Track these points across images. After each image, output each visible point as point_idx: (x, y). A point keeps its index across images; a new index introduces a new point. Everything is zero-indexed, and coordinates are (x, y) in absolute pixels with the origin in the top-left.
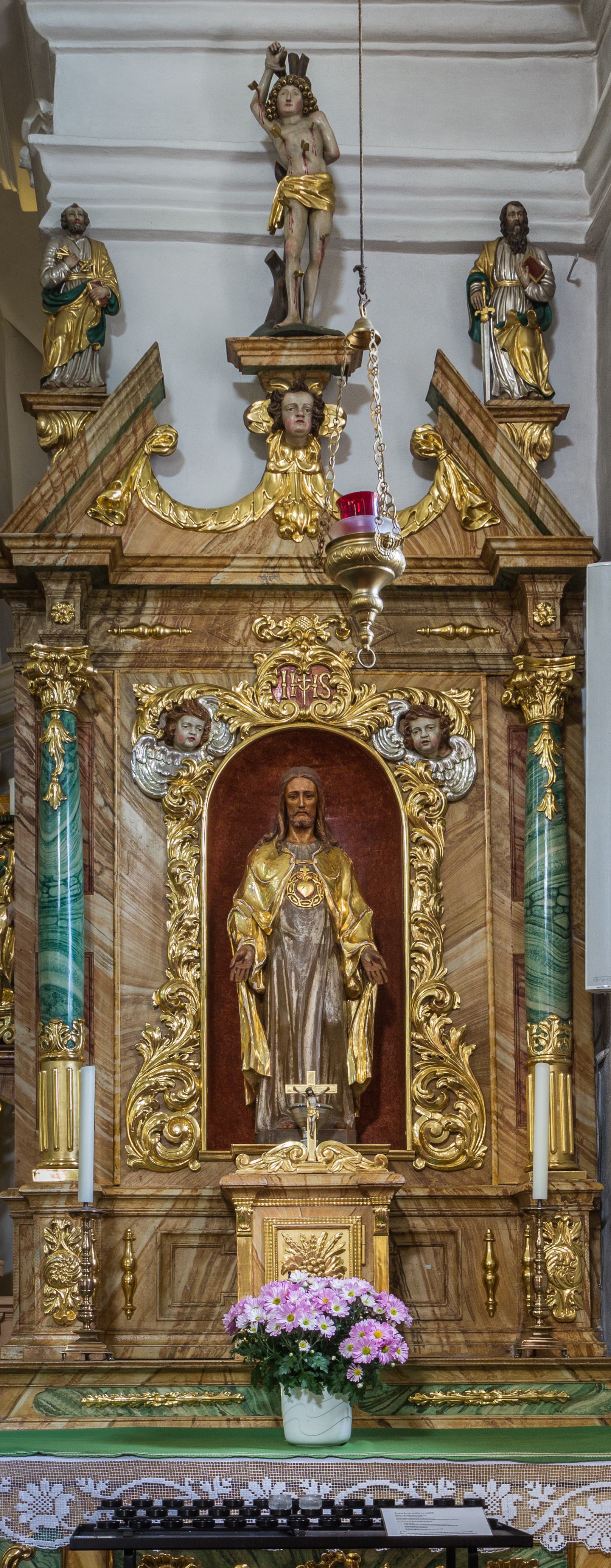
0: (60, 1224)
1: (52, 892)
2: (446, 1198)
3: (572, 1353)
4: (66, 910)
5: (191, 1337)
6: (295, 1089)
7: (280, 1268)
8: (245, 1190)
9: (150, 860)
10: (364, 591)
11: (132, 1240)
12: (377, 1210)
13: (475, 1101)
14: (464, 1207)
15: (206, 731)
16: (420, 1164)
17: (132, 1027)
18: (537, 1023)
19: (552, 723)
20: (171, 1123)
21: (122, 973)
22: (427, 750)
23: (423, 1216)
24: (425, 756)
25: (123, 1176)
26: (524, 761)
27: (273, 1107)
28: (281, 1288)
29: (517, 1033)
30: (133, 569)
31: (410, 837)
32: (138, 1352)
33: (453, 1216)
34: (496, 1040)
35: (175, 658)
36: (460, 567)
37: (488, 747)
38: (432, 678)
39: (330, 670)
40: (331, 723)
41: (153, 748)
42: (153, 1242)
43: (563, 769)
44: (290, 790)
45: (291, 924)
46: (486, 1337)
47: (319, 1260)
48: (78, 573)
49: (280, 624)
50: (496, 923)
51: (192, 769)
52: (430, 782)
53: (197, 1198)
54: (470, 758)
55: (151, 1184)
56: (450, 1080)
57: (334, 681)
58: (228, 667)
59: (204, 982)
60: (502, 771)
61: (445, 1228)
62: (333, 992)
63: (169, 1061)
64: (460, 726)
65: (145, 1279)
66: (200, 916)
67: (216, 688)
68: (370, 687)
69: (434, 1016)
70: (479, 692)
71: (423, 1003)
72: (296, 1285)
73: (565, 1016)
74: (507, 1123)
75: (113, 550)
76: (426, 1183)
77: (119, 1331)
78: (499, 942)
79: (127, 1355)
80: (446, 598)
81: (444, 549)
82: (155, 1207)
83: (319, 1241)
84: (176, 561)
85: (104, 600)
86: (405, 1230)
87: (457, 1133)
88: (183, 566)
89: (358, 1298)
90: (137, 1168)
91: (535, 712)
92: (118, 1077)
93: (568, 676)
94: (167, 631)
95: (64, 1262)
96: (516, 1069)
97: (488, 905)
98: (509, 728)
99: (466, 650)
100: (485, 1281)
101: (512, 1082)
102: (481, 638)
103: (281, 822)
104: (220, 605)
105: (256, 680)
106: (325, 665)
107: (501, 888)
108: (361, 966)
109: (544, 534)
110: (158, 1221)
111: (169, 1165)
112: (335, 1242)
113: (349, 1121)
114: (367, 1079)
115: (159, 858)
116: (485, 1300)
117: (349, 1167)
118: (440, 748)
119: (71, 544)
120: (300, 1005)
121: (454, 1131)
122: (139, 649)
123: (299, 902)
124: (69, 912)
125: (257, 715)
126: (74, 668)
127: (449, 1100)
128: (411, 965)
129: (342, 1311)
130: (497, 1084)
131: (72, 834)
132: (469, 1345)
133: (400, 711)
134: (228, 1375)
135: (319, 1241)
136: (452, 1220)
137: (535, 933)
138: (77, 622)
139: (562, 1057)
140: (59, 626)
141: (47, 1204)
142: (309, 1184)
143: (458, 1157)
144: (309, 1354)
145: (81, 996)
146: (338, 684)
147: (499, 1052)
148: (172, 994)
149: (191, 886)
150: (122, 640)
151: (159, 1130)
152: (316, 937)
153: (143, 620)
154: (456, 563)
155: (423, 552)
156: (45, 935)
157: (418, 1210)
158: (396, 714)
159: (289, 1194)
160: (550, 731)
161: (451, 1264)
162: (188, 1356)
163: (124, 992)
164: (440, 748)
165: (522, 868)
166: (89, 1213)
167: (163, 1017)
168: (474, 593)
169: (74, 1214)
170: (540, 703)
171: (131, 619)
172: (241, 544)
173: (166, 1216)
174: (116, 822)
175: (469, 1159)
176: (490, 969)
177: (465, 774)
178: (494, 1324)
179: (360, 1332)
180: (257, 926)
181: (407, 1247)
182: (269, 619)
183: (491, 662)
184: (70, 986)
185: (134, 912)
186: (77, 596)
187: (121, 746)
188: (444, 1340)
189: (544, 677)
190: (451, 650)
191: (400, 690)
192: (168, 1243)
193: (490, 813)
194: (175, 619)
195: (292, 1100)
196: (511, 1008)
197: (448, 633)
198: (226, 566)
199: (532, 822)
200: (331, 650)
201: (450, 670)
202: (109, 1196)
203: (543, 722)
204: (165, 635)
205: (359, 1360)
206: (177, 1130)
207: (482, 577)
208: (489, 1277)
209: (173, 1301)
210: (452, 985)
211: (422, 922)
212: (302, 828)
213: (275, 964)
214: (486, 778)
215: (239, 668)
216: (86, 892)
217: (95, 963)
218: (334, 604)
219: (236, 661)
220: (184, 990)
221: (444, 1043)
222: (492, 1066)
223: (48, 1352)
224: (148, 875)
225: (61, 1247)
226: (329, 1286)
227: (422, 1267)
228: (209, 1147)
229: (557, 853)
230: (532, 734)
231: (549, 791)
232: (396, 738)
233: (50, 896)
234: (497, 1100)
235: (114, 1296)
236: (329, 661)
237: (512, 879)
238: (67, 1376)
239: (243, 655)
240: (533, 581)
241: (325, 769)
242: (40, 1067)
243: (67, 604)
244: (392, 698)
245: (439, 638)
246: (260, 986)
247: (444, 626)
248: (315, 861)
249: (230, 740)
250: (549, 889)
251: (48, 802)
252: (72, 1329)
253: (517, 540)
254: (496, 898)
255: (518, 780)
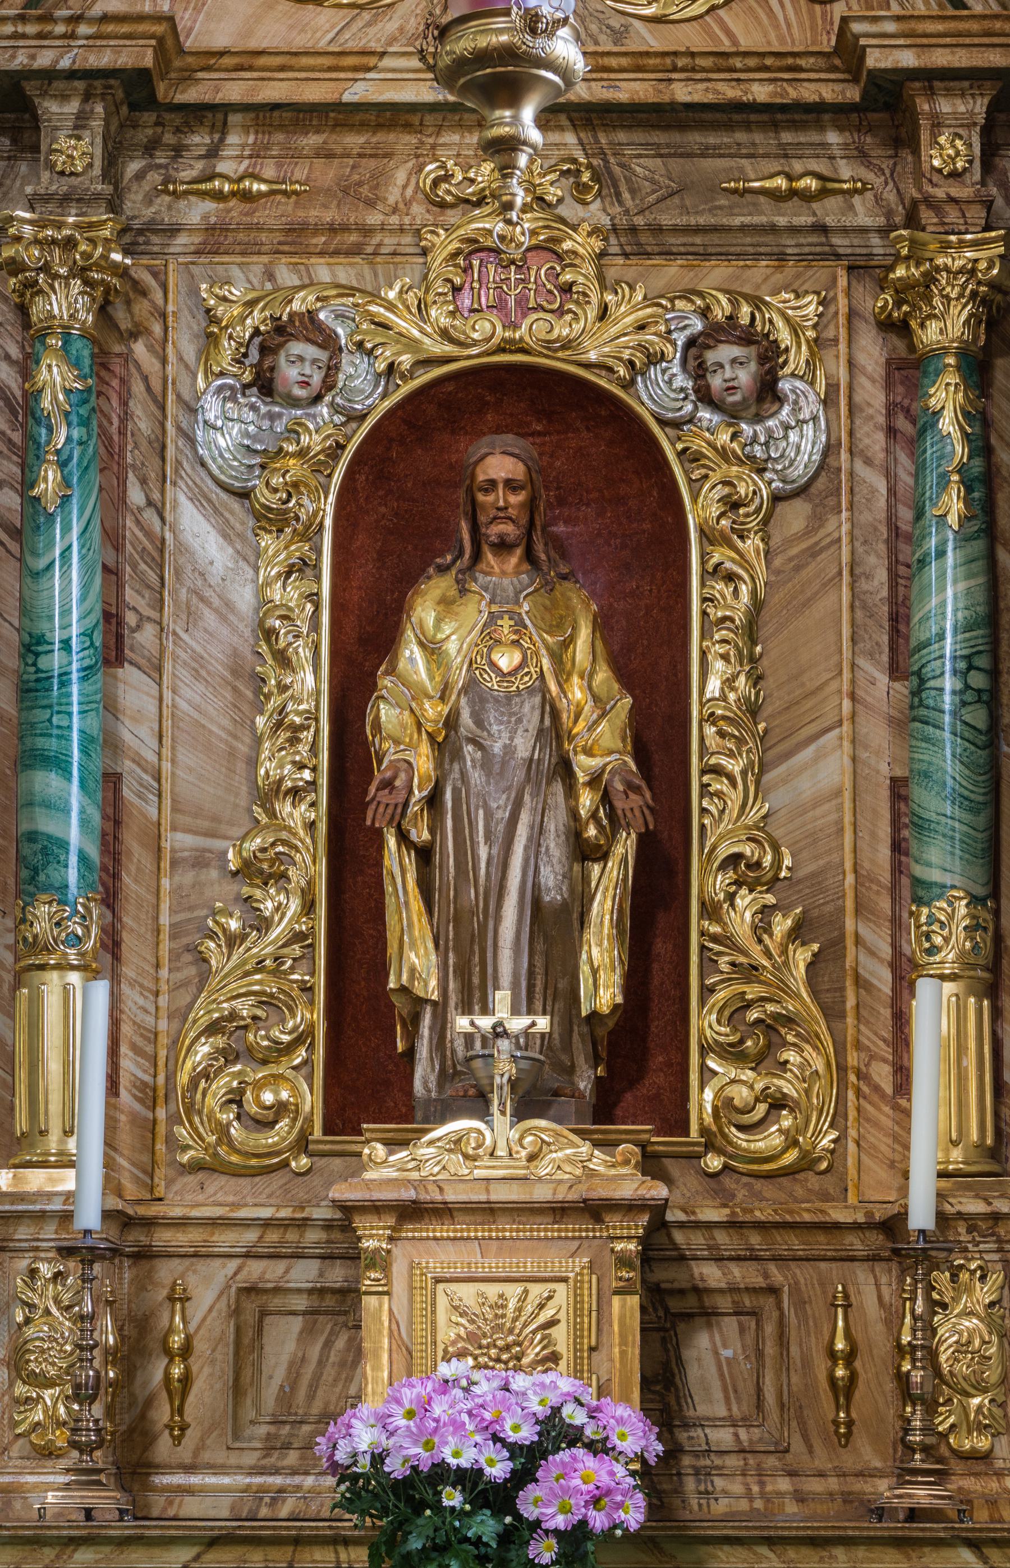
0: (46, 1270)
1: (43, 662)
2: (760, 1226)
3: (982, 1515)
4: (69, 695)
5: (289, 1481)
6: (472, 1024)
7: (440, 1354)
8: (376, 1208)
9: (229, 605)
10: (507, 113)
11: (185, 1300)
12: (619, 1246)
13: (815, 1048)
14: (795, 1243)
15: (332, 370)
16: (714, 1162)
17: (191, 908)
18: (928, 904)
19: (963, 354)
20: (259, 1086)
21: (174, 810)
22: (734, 404)
23: (719, 1259)
24: (733, 414)
25: (170, 1182)
26: (914, 422)
27: (443, 1057)
28: (419, 1389)
29: (896, 924)
30: (200, 75)
31: (703, 562)
32: (191, 1507)
33: (774, 1259)
34: (857, 935)
35: (279, 237)
36: (799, 69)
37: (850, 398)
38: (749, 272)
39: (559, 257)
40: (560, 354)
41: (235, 401)
42: (222, 1305)
43: (986, 439)
44: (481, 477)
45: (479, 723)
46: (833, 1483)
47: (510, 1338)
48: (98, 83)
49: (472, 175)
50: (860, 719)
51: (305, 440)
52: (741, 463)
53: (303, 1224)
54: (815, 418)
55: (220, 1197)
56: (770, 1008)
57: (568, 277)
58: (375, 254)
59: (322, 827)
60: (875, 441)
61: (759, 1281)
62: (555, 846)
63: (257, 971)
64: (797, 359)
65: (207, 1370)
66: (317, 707)
67: (350, 291)
68: (632, 288)
69: (744, 891)
70: (835, 298)
71: (723, 867)
72: (446, 1385)
73: (980, 891)
74: (877, 1088)
75: (161, 40)
76: (725, 1198)
77: (158, 1466)
78: (864, 755)
79: (171, 1512)
80: (776, 126)
81: (773, 36)
82: (226, 1240)
83: (512, 1305)
84: (278, 61)
85: (150, 132)
86: (685, 1285)
87: (783, 1107)
88: (291, 69)
89: (556, 1410)
90: (196, 1167)
91: (931, 334)
92: (163, 1001)
93: (990, 267)
94: (264, 187)
95: (52, 1339)
96: (894, 989)
97: (846, 687)
98: (888, 362)
99: (810, 220)
100: (832, 1380)
101: (886, 1013)
102: (840, 198)
103: (466, 536)
104: (361, 140)
105: (425, 277)
106: (549, 248)
107: (871, 655)
108: (606, 798)
109: (956, 7)
110: (233, 1265)
111: (254, 1162)
112: (541, 1306)
113: (584, 1084)
114: (616, 1006)
115: (244, 598)
116: (831, 1416)
117: (568, 1169)
118: (760, 399)
119: (83, 29)
120: (493, 870)
121: (778, 1103)
122: (213, 220)
123: (493, 682)
124: (75, 698)
125: (426, 340)
126: (87, 256)
127: (769, 1045)
128: (702, 797)
129: (526, 1434)
130: (858, 1017)
131: (82, 558)
132: (800, 1497)
133: (688, 332)
134: (341, 1549)
135: (512, 1305)
136: (772, 1268)
137: (927, 740)
138: (97, 171)
139: (973, 967)
140: (64, 180)
141: (23, 1232)
142: (493, 1197)
143: (784, 1151)
144: (463, 1514)
145: (94, 853)
146: (572, 284)
147: (862, 958)
148: (263, 850)
149: (303, 652)
150: (182, 204)
151: (235, 1099)
152: (523, 746)
153: (222, 167)
154: (790, 61)
155: (735, 42)
156: (28, 741)
157: (710, 1248)
158: (681, 339)
159: (459, 1217)
160: (958, 368)
161: (770, 1349)
162: (284, 1513)
163: (177, 845)
164: (760, 399)
165: (908, 619)
166: (91, 1249)
167: (246, 891)
168: (826, 117)
169: (66, 1252)
170: (942, 317)
171: (199, 165)
172: (401, 29)
173: (247, 1256)
174: (168, 535)
175: (805, 1155)
176: (848, 805)
177: (806, 446)
178: (848, 1461)
179: (555, 1472)
180: (419, 725)
181: (690, 1316)
182: (450, 164)
183: (856, 242)
184: (74, 835)
185: (198, 699)
186: (97, 124)
187: (179, 396)
188: (756, 1489)
189: (947, 269)
190: (782, 221)
191: (687, 294)
192: (251, 1307)
193: (851, 520)
194: (279, 166)
195: (478, 1044)
196: (885, 877)
197: (778, 189)
198: (369, 69)
199: (924, 536)
200: (563, 221)
201: (781, 257)
202: (143, 1218)
203: (945, 350)
204: (261, 195)
205: (551, 1525)
206: (268, 1097)
207: (838, 87)
208: (840, 1372)
209: (259, 1412)
210: (777, 834)
211: (724, 718)
212: (503, 547)
213: (448, 796)
214: (844, 456)
215: (394, 254)
216: (107, 662)
217: (126, 792)
218: (570, 138)
219: (390, 242)
220: (284, 843)
221: (760, 941)
222: (849, 983)
223: (18, 1505)
224: (224, 631)
225: (47, 1312)
226: (506, 1388)
227: (716, 1353)
228: (327, 1130)
229: (968, 592)
230: (926, 374)
231: (955, 478)
232: (681, 381)
233: (38, 671)
234: (858, 1046)
235: (149, 1402)
236: (558, 241)
237: (891, 640)
238: (47, 1550)
239: (402, 230)
240: (931, 93)
241: (555, 438)
242: (17, 984)
243: (79, 138)
244: (673, 309)
245: (762, 199)
246: (421, 834)
247: (771, 176)
248: (526, 607)
249: (376, 386)
250: (954, 658)
251: (37, 499)
252: (63, 1463)
253: (898, 18)
254: (859, 674)
255: (903, 458)
